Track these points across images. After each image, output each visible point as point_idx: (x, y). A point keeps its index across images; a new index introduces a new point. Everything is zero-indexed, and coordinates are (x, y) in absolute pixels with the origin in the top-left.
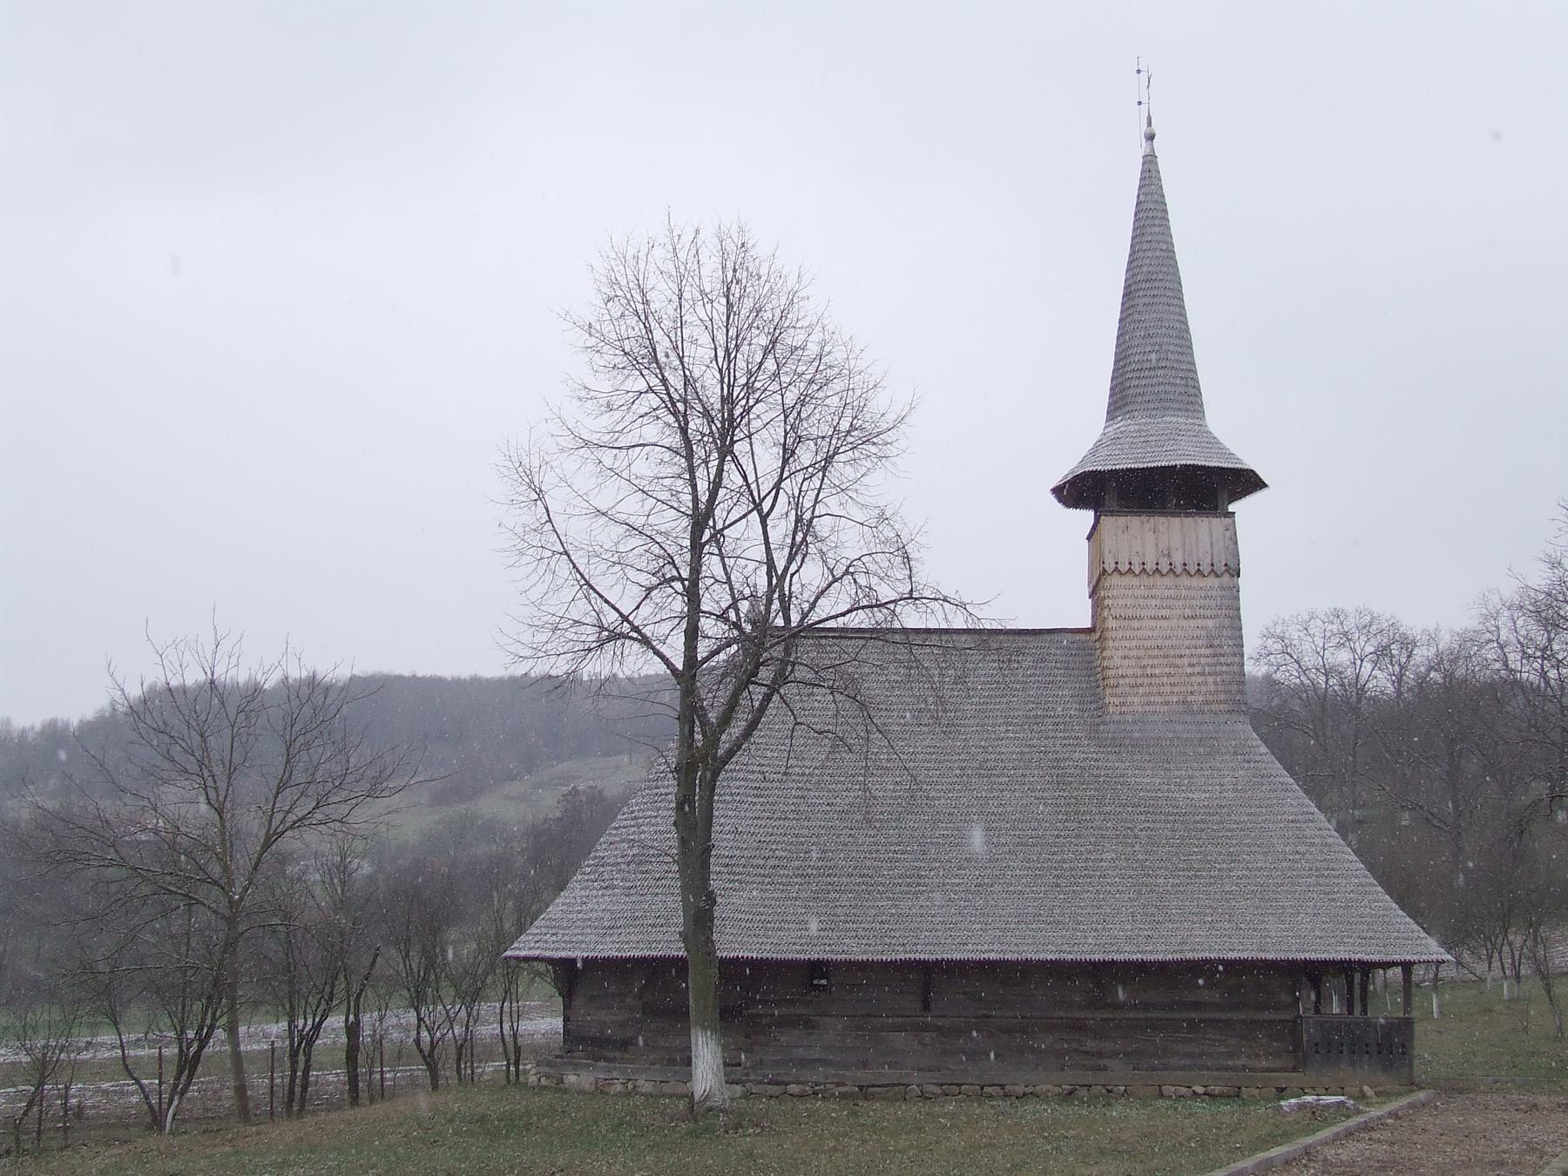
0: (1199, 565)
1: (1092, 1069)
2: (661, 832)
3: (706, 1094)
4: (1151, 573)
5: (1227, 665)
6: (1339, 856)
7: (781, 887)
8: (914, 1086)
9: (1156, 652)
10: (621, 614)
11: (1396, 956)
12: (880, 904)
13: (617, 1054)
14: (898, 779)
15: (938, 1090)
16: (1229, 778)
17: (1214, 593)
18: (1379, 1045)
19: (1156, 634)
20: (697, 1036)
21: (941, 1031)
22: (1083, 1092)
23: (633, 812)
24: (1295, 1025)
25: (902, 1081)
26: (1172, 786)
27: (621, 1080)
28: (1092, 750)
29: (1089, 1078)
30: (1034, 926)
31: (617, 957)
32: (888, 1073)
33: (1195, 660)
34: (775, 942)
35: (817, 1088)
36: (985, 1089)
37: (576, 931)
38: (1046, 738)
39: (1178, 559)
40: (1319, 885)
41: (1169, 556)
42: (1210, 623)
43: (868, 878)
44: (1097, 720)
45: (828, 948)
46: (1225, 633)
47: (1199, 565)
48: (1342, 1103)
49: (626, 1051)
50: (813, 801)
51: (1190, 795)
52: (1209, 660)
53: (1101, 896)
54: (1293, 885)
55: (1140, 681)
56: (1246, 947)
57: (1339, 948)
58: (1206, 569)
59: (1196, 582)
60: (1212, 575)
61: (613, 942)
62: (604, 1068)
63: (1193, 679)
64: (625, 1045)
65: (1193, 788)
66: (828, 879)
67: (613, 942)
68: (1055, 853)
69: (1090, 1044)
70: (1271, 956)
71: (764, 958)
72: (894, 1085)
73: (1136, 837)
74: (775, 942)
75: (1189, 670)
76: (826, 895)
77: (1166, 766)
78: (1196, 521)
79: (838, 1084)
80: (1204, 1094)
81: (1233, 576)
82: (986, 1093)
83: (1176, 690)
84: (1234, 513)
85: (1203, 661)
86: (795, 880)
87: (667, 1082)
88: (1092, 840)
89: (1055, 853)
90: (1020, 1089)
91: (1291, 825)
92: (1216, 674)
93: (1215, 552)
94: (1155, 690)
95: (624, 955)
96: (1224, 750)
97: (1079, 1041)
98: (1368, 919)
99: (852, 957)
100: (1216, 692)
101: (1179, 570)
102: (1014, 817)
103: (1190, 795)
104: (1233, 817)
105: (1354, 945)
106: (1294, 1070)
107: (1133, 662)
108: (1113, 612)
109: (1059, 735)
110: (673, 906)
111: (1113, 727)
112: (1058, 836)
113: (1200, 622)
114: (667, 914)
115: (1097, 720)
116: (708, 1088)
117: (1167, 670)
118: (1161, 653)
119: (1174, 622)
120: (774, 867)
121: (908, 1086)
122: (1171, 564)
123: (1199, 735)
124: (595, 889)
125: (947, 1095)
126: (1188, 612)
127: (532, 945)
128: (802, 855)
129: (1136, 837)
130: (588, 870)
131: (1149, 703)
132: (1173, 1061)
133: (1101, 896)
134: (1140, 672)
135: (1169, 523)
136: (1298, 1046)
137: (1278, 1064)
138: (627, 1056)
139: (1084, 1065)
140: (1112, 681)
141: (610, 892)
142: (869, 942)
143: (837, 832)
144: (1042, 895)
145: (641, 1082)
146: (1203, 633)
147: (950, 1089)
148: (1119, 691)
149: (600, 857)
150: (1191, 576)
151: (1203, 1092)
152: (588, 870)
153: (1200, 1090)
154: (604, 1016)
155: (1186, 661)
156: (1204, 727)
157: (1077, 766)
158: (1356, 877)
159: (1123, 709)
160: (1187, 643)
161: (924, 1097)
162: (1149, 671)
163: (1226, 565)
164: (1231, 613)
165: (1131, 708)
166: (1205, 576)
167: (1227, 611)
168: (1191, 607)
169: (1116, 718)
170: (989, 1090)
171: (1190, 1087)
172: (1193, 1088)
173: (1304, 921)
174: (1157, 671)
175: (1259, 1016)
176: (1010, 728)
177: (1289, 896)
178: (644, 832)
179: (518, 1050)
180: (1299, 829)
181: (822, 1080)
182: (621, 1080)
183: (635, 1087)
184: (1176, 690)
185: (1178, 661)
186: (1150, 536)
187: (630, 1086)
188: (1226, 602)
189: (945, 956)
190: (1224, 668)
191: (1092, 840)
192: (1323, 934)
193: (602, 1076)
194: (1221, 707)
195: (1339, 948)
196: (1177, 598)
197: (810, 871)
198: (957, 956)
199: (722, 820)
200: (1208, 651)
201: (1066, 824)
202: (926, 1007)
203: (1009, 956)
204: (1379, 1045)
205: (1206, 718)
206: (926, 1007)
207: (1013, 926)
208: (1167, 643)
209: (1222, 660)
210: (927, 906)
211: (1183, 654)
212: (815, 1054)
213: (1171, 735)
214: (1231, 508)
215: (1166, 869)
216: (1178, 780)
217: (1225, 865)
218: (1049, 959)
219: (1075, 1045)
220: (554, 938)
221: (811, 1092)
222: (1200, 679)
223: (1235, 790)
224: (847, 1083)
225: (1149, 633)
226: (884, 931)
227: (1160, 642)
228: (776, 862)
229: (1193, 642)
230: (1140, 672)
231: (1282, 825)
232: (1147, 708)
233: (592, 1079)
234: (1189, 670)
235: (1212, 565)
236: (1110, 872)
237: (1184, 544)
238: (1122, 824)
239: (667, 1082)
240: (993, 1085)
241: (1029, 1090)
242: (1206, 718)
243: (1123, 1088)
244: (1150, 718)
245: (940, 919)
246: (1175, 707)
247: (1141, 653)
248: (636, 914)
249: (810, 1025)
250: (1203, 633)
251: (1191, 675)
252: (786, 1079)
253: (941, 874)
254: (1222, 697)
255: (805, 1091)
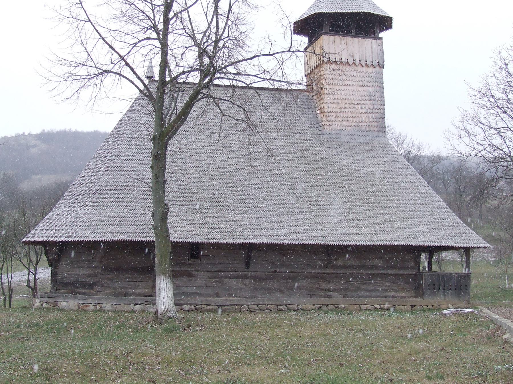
0: (366, 61)
1: (325, 297)
2: (111, 179)
3: (166, 310)
4: (345, 64)
5: (378, 109)
6: (435, 199)
7: (178, 206)
8: (245, 305)
9: (346, 101)
10: (120, 56)
11: (467, 245)
12: (228, 216)
13: (87, 291)
14: (229, 156)
15: (256, 307)
16: (381, 161)
17: (372, 75)
18: (455, 286)
19: (346, 92)
20: (160, 279)
21: (255, 279)
22: (325, 308)
23: (91, 169)
24: (419, 275)
25: (264, 303)
26: (357, 164)
27: (93, 304)
28: (318, 146)
29: (327, 301)
30: (303, 228)
31: (95, 240)
32: (233, 300)
33: (363, 106)
34: (179, 234)
35: (197, 307)
36: (279, 307)
37: (68, 228)
38: (297, 139)
39: (357, 58)
40: (428, 211)
41: (353, 56)
42: (371, 89)
43: (220, 203)
44: (319, 132)
45: (206, 237)
46: (377, 94)
47: (366, 61)
48: (472, 312)
49: (92, 289)
50: (189, 165)
51: (365, 169)
52: (370, 107)
53: (332, 214)
54: (417, 211)
55: (339, 115)
56: (402, 239)
57: (442, 241)
58: (369, 63)
59: (365, 69)
60: (372, 67)
61: (91, 233)
62: (82, 298)
63: (362, 115)
64: (91, 286)
65: (366, 166)
66: (201, 203)
67: (91, 233)
68: (308, 194)
69: (323, 285)
70: (413, 244)
71: (175, 241)
72: (234, 305)
73: (344, 187)
74: (179, 234)
75: (361, 111)
76: (201, 211)
77: (352, 155)
78: (365, 41)
79: (208, 305)
80: (380, 309)
81: (381, 68)
82: (280, 309)
83: (355, 120)
84: (382, 38)
85: (367, 107)
86: (185, 203)
87: (119, 305)
88: (324, 188)
89: (308, 194)
90: (295, 307)
91: (412, 184)
92: (373, 113)
93: (373, 56)
94: (345, 119)
95: (99, 240)
96: (377, 148)
97: (319, 284)
98: (451, 227)
99: (219, 241)
100: (373, 122)
101: (357, 63)
102: (286, 176)
103: (365, 169)
104: (386, 179)
105: (448, 239)
106: (416, 297)
107: (335, 105)
108: (327, 81)
109: (302, 138)
110: (122, 215)
111: (326, 136)
112: (308, 186)
113: (366, 88)
114: (119, 219)
115: (319, 132)
116: (167, 307)
117: (351, 110)
118: (349, 102)
119: (354, 88)
120: (174, 197)
121: (242, 305)
122: (354, 60)
123: (365, 141)
124: (74, 206)
125: (261, 310)
126: (360, 83)
127: (41, 235)
128: (186, 191)
129: (344, 187)
130: (68, 197)
131: (343, 125)
132: (363, 293)
133: (332, 214)
134: (338, 110)
135: (353, 40)
136: (420, 285)
137: (408, 294)
138: (92, 291)
139: (321, 295)
140: (326, 114)
141: (84, 208)
142: (226, 234)
143: (203, 180)
144: (304, 213)
145: (104, 305)
146: (367, 94)
147: (261, 308)
148: (329, 118)
149: (74, 191)
150: (363, 66)
151: (379, 308)
152: (68, 197)
153: (378, 307)
154: (78, 271)
155: (359, 106)
156: (368, 138)
157: (313, 153)
158: (443, 208)
159: (331, 127)
160: (360, 98)
161: (250, 311)
162: (343, 110)
163: (378, 62)
164: (380, 85)
165: (334, 127)
166: (369, 67)
167: (378, 84)
168: (362, 81)
169: (328, 132)
170: (281, 307)
171: (373, 305)
172: (374, 306)
173: (424, 228)
174: (346, 110)
175: (401, 272)
176: (279, 134)
177: (416, 216)
178: (101, 178)
179: (11, 291)
180: (415, 186)
181: (200, 303)
182: (93, 304)
183: (101, 307)
184: (355, 120)
185: (356, 106)
186: (344, 46)
187: (98, 307)
188: (378, 80)
189: (263, 241)
190: (377, 111)
191: (324, 188)
192: (434, 234)
193: (82, 302)
194: (375, 129)
195: (442, 241)
196: (356, 77)
197: (191, 199)
198: (270, 241)
199: (144, 173)
200: (370, 102)
201: (311, 180)
202: (247, 265)
203: (294, 242)
204: (455, 286)
205: (368, 133)
206: (247, 265)
207: (294, 228)
208: (351, 97)
209: (376, 107)
210: (251, 217)
211: (358, 103)
212: (194, 290)
213: (353, 141)
214: (381, 35)
215: (359, 202)
216: (359, 162)
217: (385, 202)
218: (313, 244)
219: (317, 286)
220: (54, 231)
221: (194, 309)
222: (366, 115)
223: (385, 167)
224: (212, 304)
225: (343, 92)
226: (173, 238)
227: (348, 97)
228: (174, 194)
229: (363, 98)
230: (338, 110)
231: (408, 184)
232: (342, 128)
233: (76, 304)
234: (361, 111)
235: (372, 62)
236: (334, 203)
237: (359, 52)
238: (337, 181)
239: (119, 305)
240: (282, 305)
241: (300, 307)
242: (368, 133)
243: (343, 306)
244: (343, 132)
245: (258, 223)
246: (355, 128)
247: (340, 101)
248: (102, 219)
249: (190, 275)
250: (367, 94)
251: (361, 113)
252: (182, 302)
253: (255, 202)
254: (375, 124)
255: (192, 308)
